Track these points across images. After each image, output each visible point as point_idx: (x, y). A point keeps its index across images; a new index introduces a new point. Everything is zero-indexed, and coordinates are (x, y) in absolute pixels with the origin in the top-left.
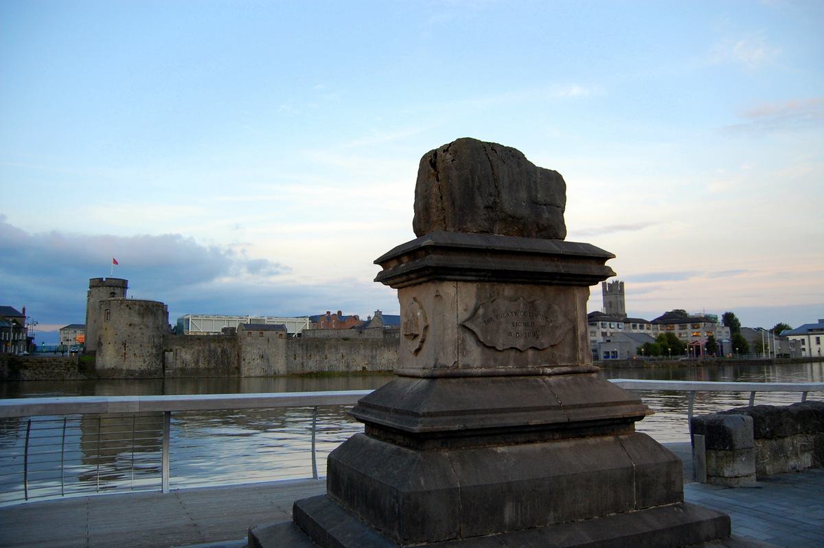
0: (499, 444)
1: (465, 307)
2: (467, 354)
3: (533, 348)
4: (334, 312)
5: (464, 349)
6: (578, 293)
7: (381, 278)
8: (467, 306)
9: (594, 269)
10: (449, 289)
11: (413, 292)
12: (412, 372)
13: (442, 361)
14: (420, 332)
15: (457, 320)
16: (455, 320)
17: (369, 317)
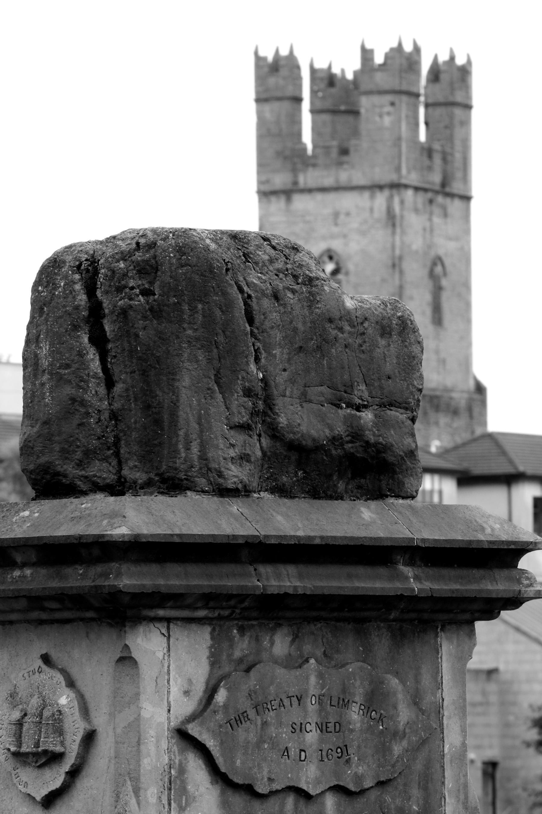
1: (186, 687)
2: (187, 804)
5: (183, 790)
8: (190, 681)
9: (496, 585)
15: (169, 719)
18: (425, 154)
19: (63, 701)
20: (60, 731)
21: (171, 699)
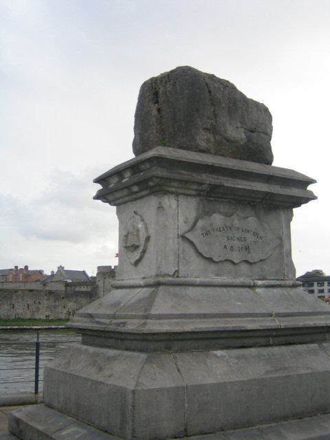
0: (217, 349)
3: (246, 262)
4: (21, 266)
6: (283, 215)
7: (100, 196)
9: (295, 192)
10: (169, 202)
11: (132, 207)
12: (131, 282)
13: (164, 270)
14: (142, 242)
16: (176, 231)
17: (53, 272)
18: (253, 127)
19: (140, 226)
20: (138, 235)
21: (179, 224)
